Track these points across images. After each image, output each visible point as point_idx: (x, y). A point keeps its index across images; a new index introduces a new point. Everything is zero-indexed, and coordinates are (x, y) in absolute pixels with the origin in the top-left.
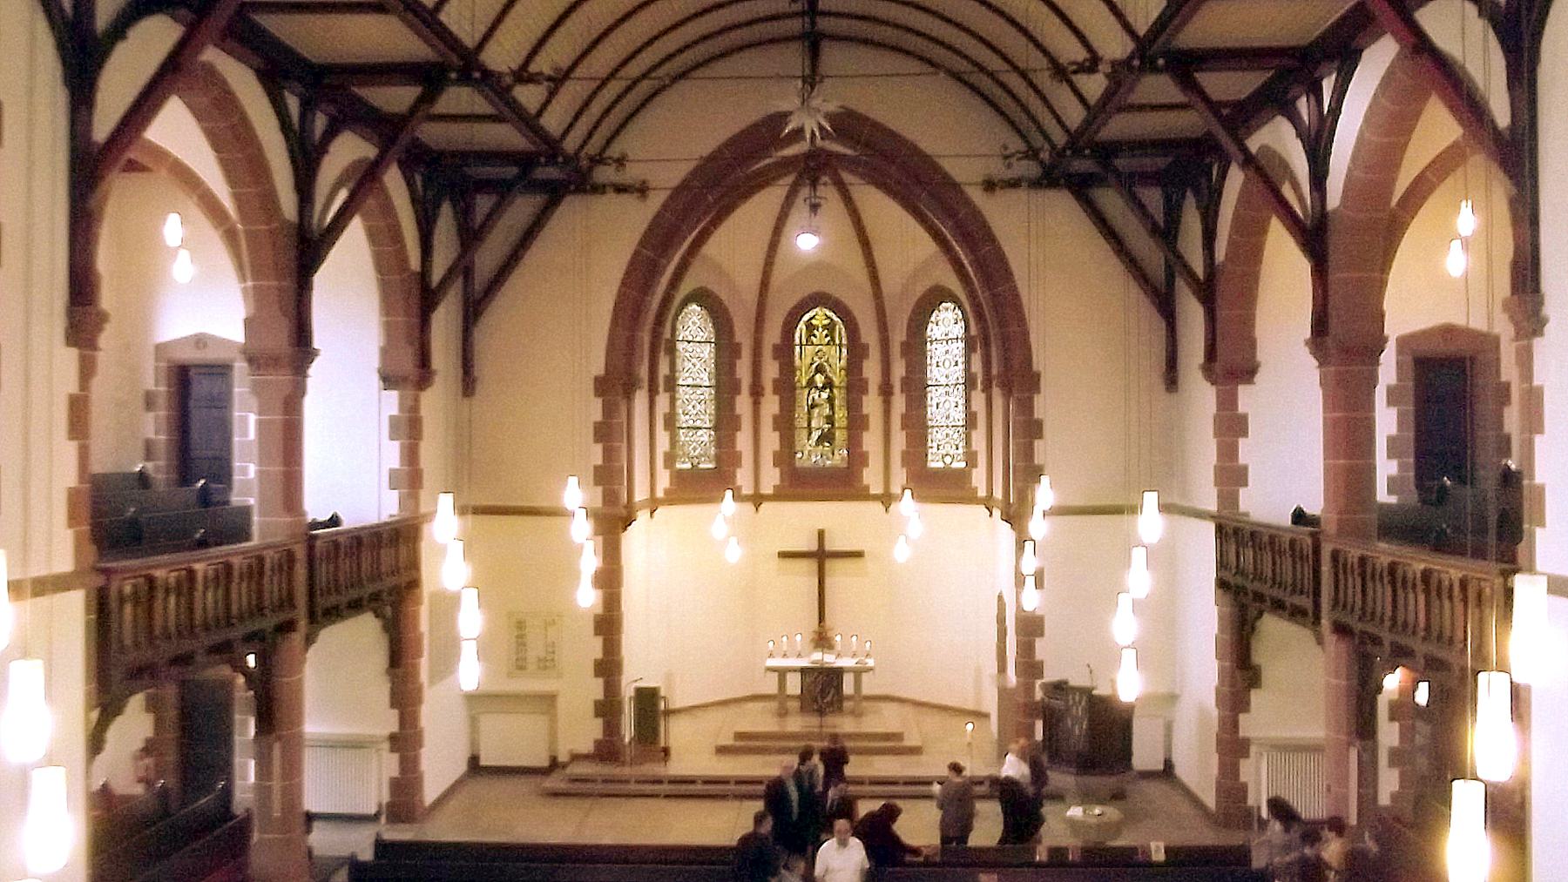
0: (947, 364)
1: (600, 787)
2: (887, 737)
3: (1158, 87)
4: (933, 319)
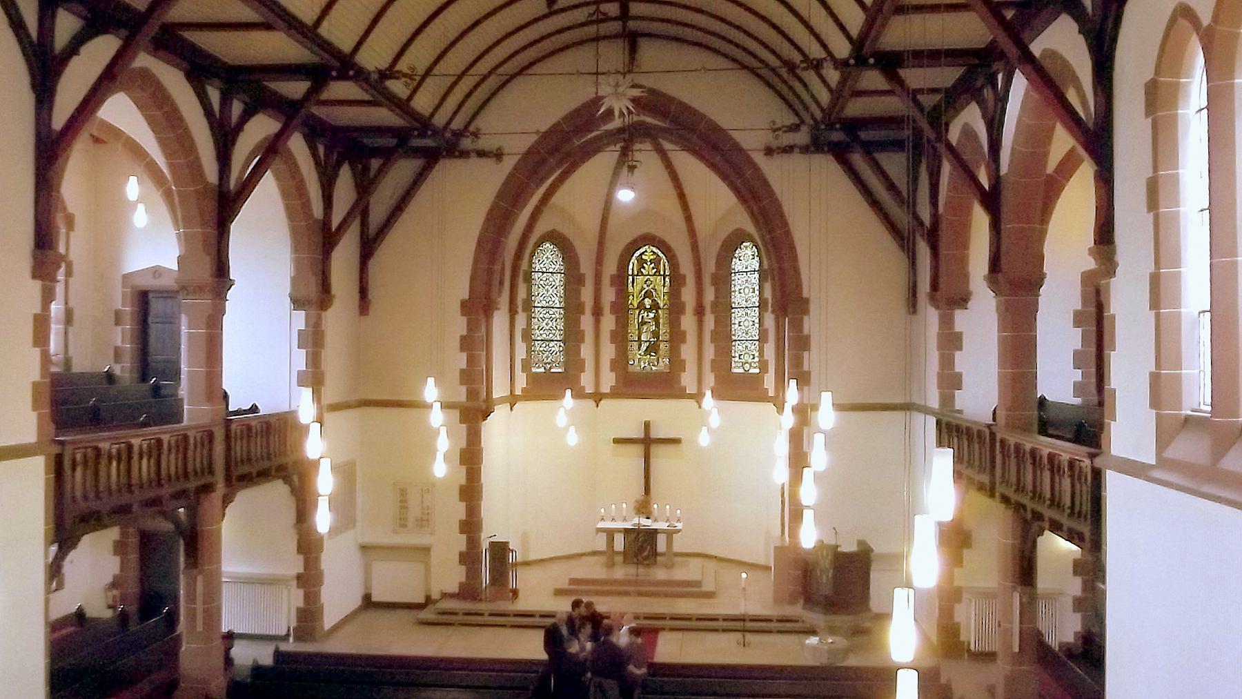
0: (747, 290)
1: (460, 618)
2: (688, 584)
3: (873, 79)
4: (736, 255)
